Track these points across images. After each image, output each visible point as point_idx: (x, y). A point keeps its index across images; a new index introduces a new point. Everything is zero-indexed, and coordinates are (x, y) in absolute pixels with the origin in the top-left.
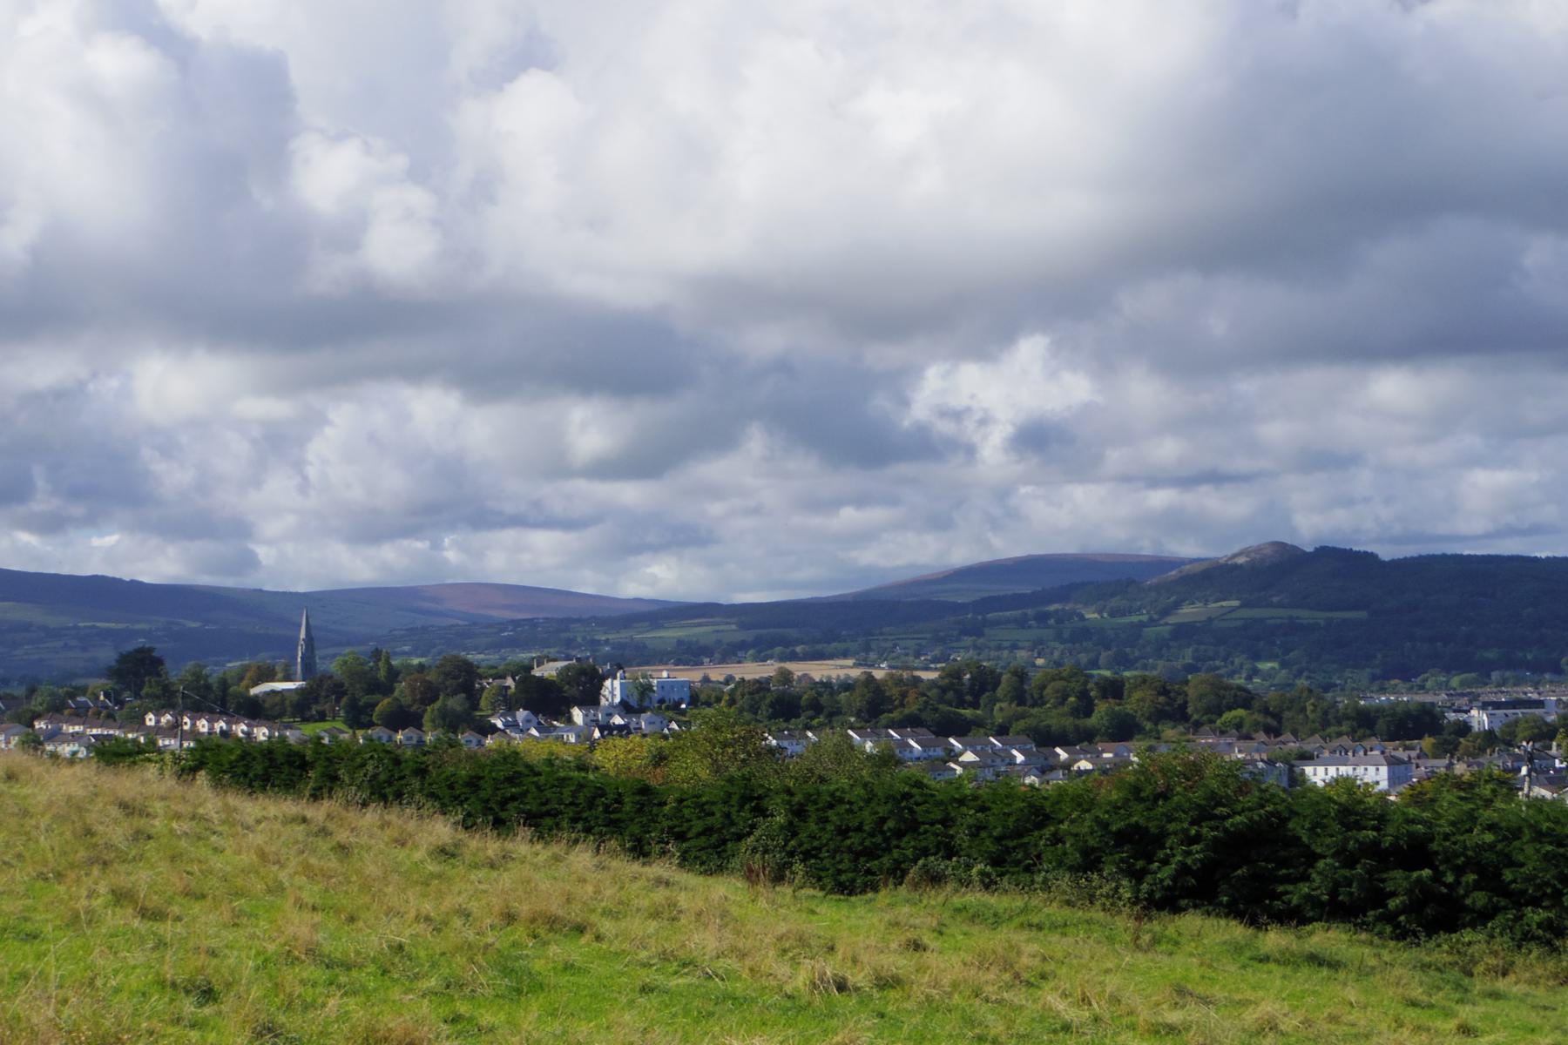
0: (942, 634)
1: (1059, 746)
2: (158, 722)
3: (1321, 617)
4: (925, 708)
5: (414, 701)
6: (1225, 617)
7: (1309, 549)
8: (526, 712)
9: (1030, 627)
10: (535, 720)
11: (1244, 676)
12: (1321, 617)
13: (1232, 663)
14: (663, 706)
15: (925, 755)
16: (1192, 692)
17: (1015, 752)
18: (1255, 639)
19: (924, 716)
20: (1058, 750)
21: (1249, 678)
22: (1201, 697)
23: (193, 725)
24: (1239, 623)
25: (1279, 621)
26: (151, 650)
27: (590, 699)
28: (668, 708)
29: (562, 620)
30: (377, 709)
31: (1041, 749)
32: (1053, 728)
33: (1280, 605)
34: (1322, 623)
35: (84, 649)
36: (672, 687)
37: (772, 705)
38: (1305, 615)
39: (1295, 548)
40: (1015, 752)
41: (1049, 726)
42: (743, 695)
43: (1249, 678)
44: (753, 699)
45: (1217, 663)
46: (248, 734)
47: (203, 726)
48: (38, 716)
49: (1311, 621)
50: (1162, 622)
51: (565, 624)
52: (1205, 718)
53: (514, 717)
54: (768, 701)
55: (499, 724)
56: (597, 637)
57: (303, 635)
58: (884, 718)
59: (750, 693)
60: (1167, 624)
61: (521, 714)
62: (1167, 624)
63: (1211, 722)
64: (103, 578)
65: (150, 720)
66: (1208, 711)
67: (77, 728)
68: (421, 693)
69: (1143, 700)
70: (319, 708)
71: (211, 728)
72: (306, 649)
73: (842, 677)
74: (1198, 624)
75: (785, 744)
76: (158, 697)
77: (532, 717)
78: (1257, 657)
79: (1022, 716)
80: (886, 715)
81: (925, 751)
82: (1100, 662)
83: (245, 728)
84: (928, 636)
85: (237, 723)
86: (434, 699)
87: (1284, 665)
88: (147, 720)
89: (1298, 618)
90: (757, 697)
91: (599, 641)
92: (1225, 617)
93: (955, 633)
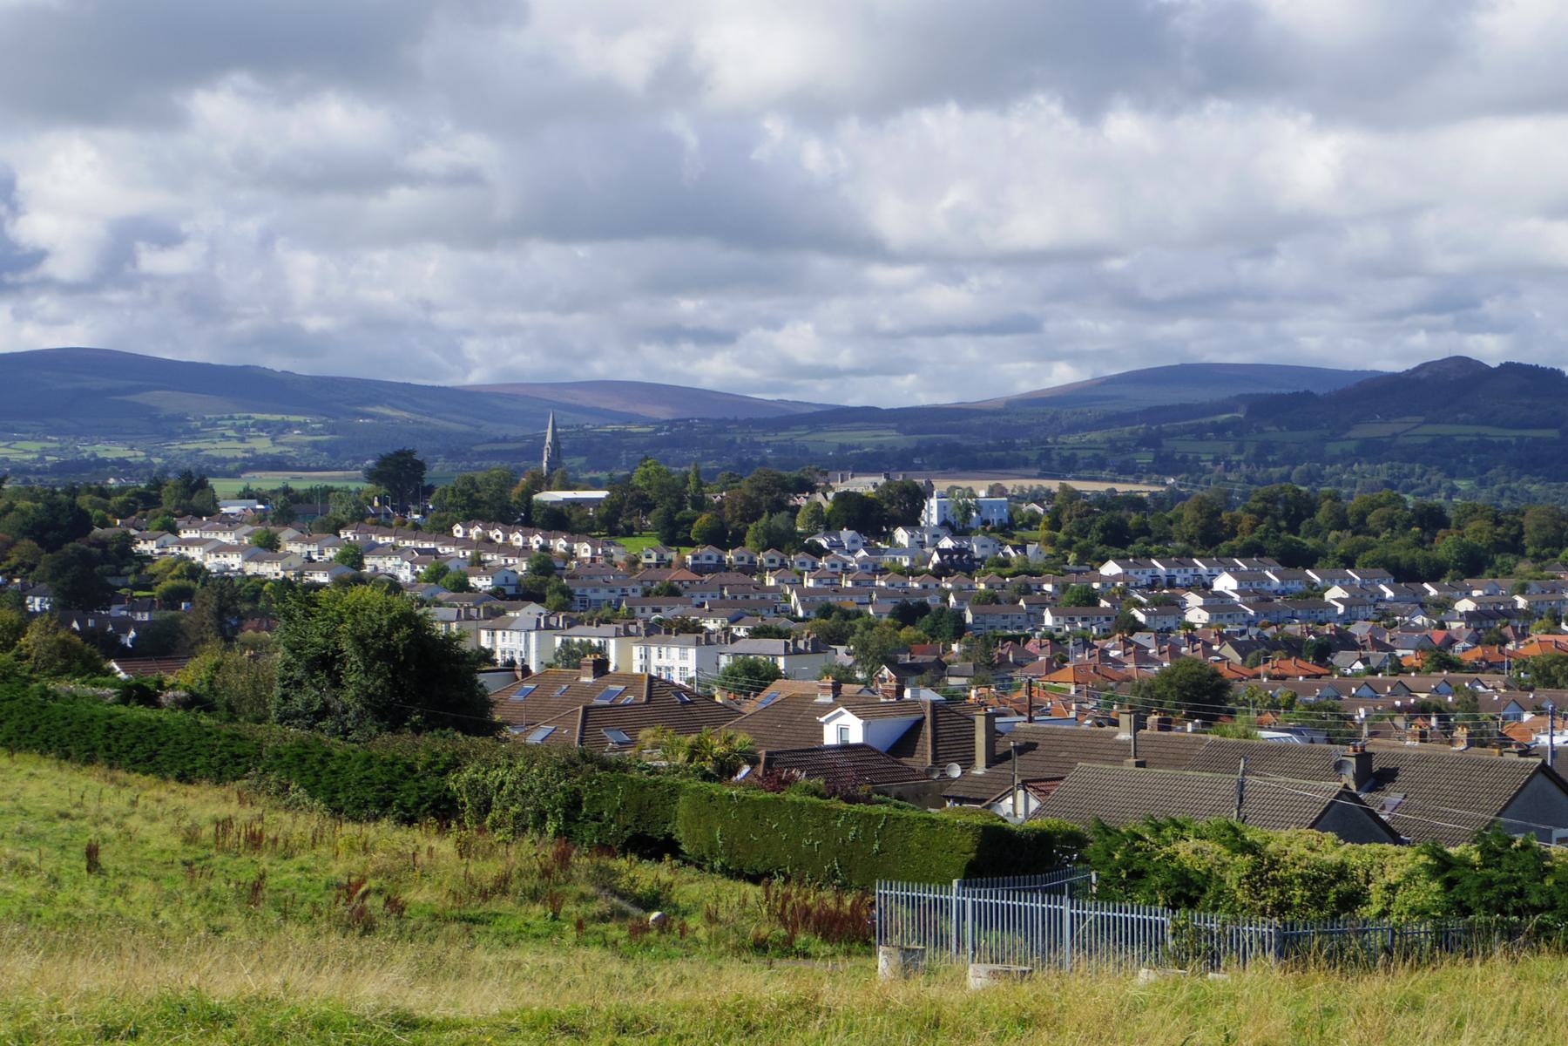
0: (1119, 444)
1: (1428, 582)
2: (466, 534)
3: (1512, 435)
4: (1267, 537)
5: (734, 517)
6: (1415, 432)
7: (1494, 364)
8: (852, 532)
9: (1209, 439)
10: (860, 541)
11: (1443, 494)
12: (1512, 435)
13: (1429, 481)
14: (988, 528)
15: (1283, 588)
16: (1529, 524)
17: (1383, 587)
18: (1449, 458)
19: (1266, 544)
20: (1426, 586)
21: (1449, 497)
22: (1540, 527)
23: (506, 538)
24: (1426, 440)
25: (1468, 439)
26: (411, 453)
27: (911, 520)
28: (993, 530)
29: (719, 421)
30: (695, 525)
31: (1409, 585)
32: (1402, 561)
33: (1466, 422)
34: (1514, 441)
35: (242, 440)
36: (991, 507)
37: (1103, 529)
38: (1494, 434)
39: (1479, 364)
40: (1383, 587)
41: (1398, 559)
42: (1070, 518)
43: (1449, 497)
44: (1081, 522)
45: (1414, 480)
46: (543, 548)
47: (518, 540)
48: (342, 525)
49: (1503, 439)
50: (1344, 437)
51: (722, 425)
52: (1546, 550)
53: (838, 536)
54: (1098, 525)
55: (824, 543)
56: (756, 439)
57: (549, 439)
58: (1224, 547)
59: (1078, 516)
60: (1350, 439)
61: (846, 535)
62: (1350, 439)
63: (1555, 556)
64: (209, 364)
65: (458, 531)
66: (1546, 543)
67: (387, 540)
68: (741, 509)
69: (1480, 531)
70: (627, 522)
71: (526, 542)
72: (553, 454)
73: (1035, 488)
74: (1385, 440)
75: (1174, 571)
76: (463, 508)
77: (857, 536)
78: (1451, 475)
79: (1365, 548)
80: (1226, 543)
81: (1282, 584)
82: (1293, 478)
83: (565, 544)
84: (1105, 446)
85: (555, 538)
86: (756, 517)
87: (1482, 483)
88: (515, 544)
89: (1486, 435)
90: (1086, 520)
91: (759, 443)
92: (1415, 432)
93: (1133, 444)
